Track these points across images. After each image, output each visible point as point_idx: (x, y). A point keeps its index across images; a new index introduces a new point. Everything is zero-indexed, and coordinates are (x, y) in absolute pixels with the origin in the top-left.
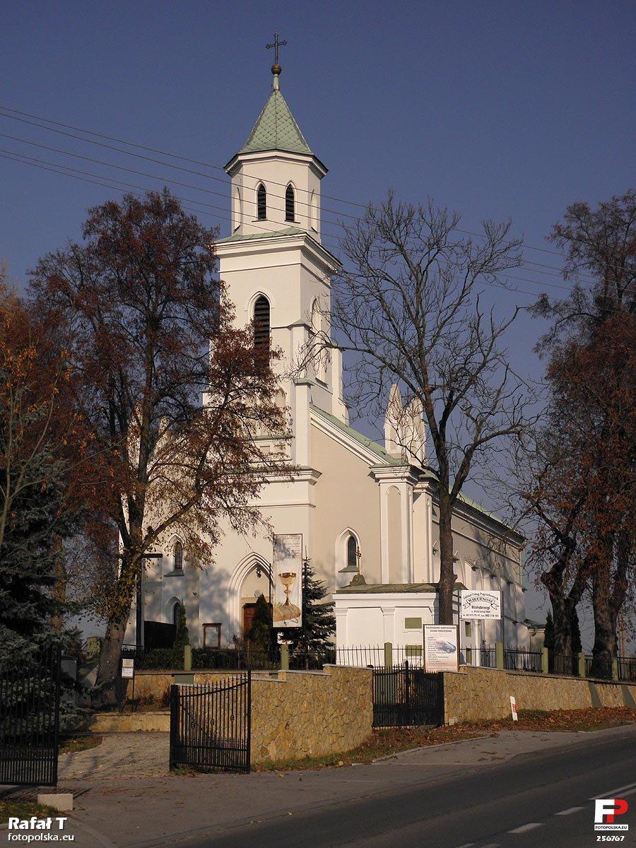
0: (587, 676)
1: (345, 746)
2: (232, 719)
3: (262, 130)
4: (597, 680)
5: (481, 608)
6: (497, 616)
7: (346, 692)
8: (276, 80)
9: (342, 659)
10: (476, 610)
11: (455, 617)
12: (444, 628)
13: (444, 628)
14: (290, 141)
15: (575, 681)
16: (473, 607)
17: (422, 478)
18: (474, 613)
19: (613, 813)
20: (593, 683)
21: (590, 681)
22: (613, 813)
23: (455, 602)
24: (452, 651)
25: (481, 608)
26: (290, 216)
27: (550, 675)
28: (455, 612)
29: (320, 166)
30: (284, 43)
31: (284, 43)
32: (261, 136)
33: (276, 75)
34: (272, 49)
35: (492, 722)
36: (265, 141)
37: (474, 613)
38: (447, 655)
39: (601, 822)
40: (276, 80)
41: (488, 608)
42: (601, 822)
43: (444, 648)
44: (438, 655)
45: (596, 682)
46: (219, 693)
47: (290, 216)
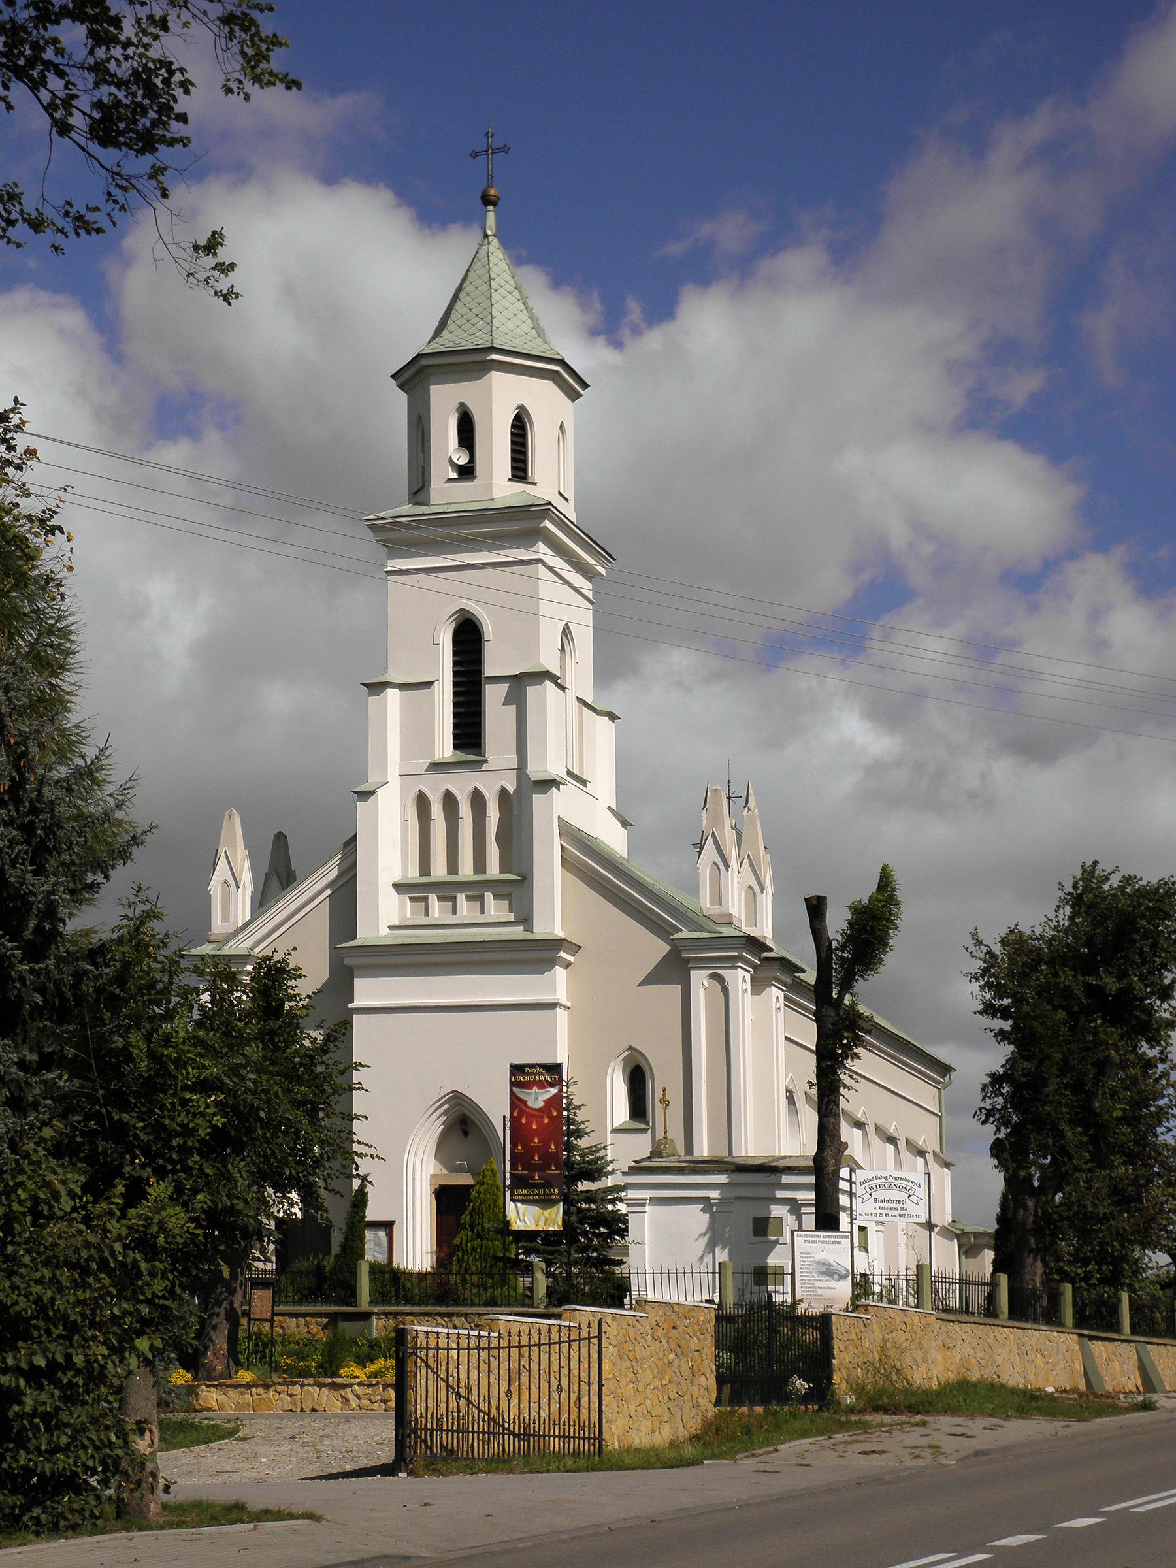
0: (1076, 1326)
1: (662, 1437)
2: (559, 1387)
3: (463, 310)
4: (1093, 1333)
5: (891, 1201)
6: (919, 1216)
7: (673, 1345)
8: (491, 217)
9: (644, 1288)
10: (883, 1205)
11: (844, 1218)
12: (829, 1236)
13: (829, 1236)
14: (518, 331)
15: (1055, 1334)
16: (876, 1199)
17: (767, 959)
18: (879, 1211)
19: (777, 1192)
20: (1086, 1339)
21: (1081, 1335)
22: (777, 1192)
23: (844, 1192)
24: (842, 1277)
25: (891, 1201)
26: (520, 470)
27: (1010, 1323)
28: (844, 1209)
29: (569, 375)
30: (505, 149)
31: (505, 149)
32: (463, 321)
33: (491, 208)
34: (482, 159)
35: (1102, 1395)
36: (470, 332)
37: (879, 1211)
38: (834, 1284)
39: (676, 990)
40: (491, 217)
41: (903, 1202)
42: (676, 990)
43: (829, 1271)
44: (818, 1284)
45: (1091, 1338)
46: (544, 1348)
47: (520, 470)
